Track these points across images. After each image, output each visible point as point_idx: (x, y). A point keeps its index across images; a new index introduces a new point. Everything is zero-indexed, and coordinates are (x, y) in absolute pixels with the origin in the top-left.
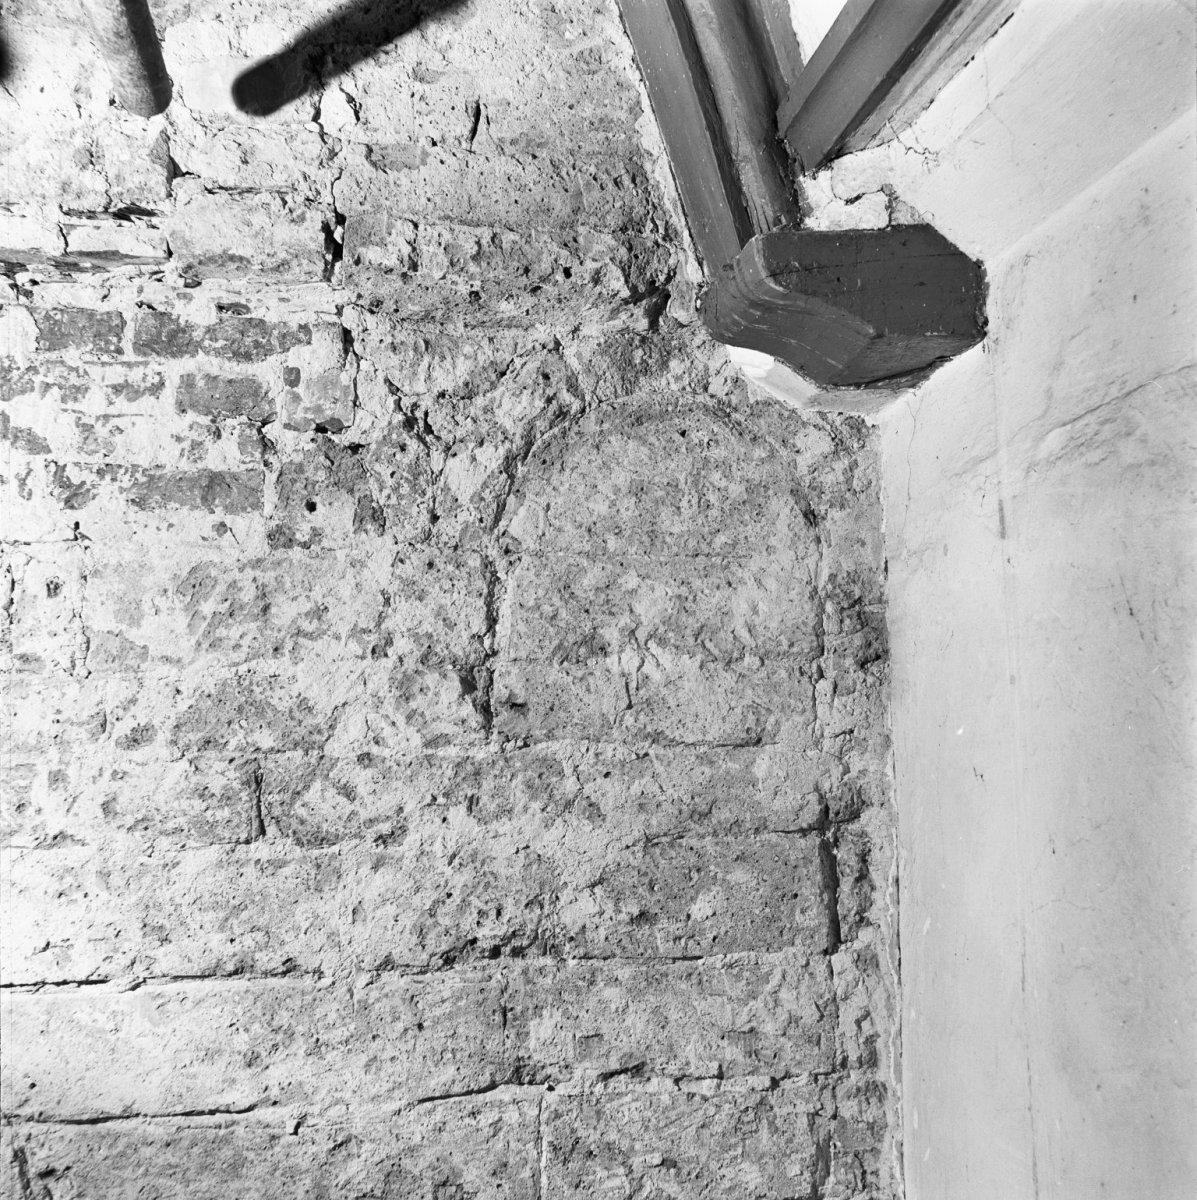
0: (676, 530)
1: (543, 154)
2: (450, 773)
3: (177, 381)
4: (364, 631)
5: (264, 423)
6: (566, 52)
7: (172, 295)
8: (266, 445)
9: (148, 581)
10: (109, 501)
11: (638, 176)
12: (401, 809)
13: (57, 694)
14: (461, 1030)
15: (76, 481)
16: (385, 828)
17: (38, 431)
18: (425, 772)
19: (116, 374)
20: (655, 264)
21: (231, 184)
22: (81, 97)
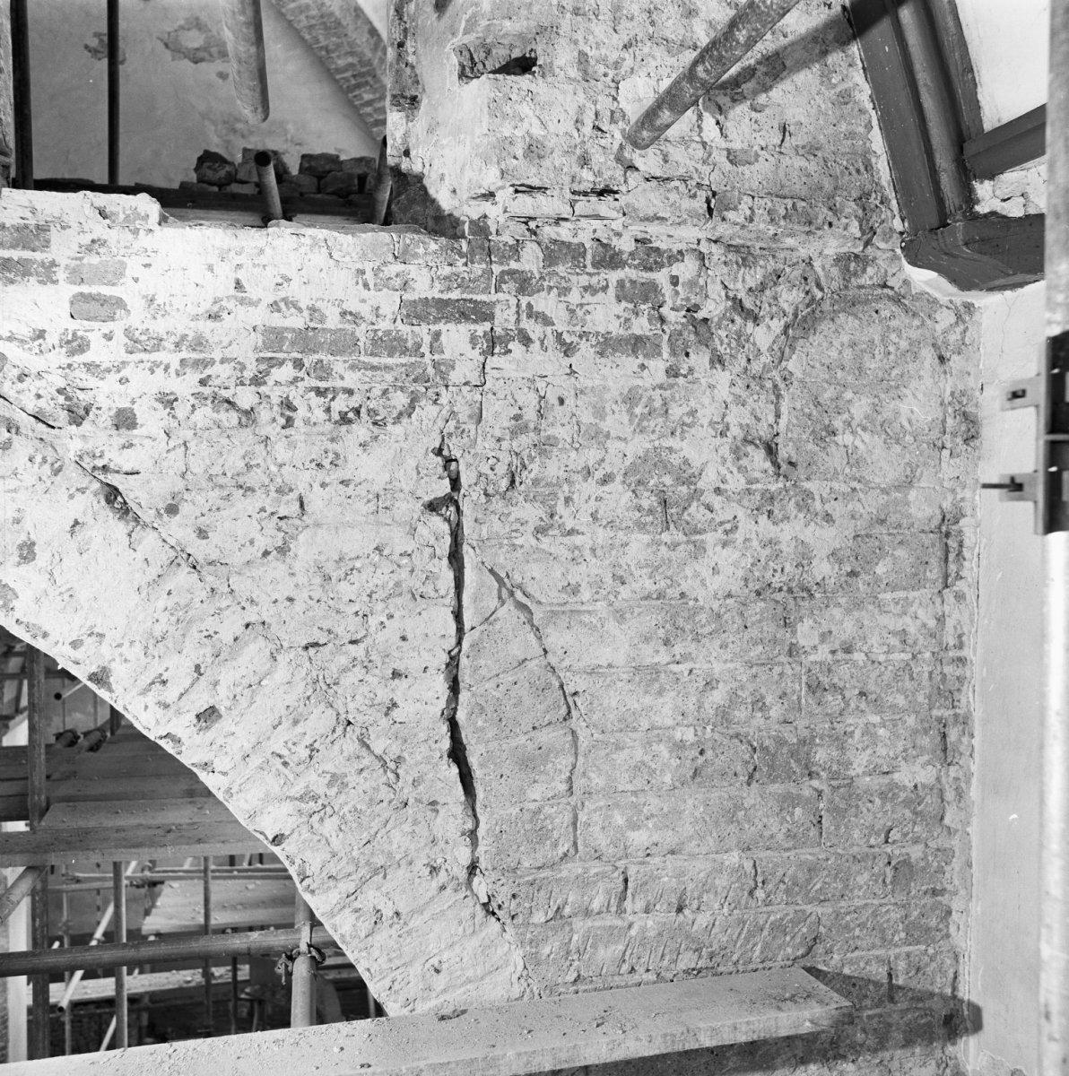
0: (872, 366)
1: (819, 154)
2: (759, 498)
3: (615, 284)
4: (716, 423)
5: (660, 307)
6: (833, 92)
7: (611, 234)
8: (662, 320)
9: (607, 396)
10: (586, 349)
11: (868, 167)
12: (735, 517)
13: (565, 457)
14: (765, 628)
15: (568, 341)
16: (728, 526)
17: (548, 313)
18: (747, 497)
19: (584, 280)
20: (874, 218)
21: (658, 175)
22: (579, 124)
